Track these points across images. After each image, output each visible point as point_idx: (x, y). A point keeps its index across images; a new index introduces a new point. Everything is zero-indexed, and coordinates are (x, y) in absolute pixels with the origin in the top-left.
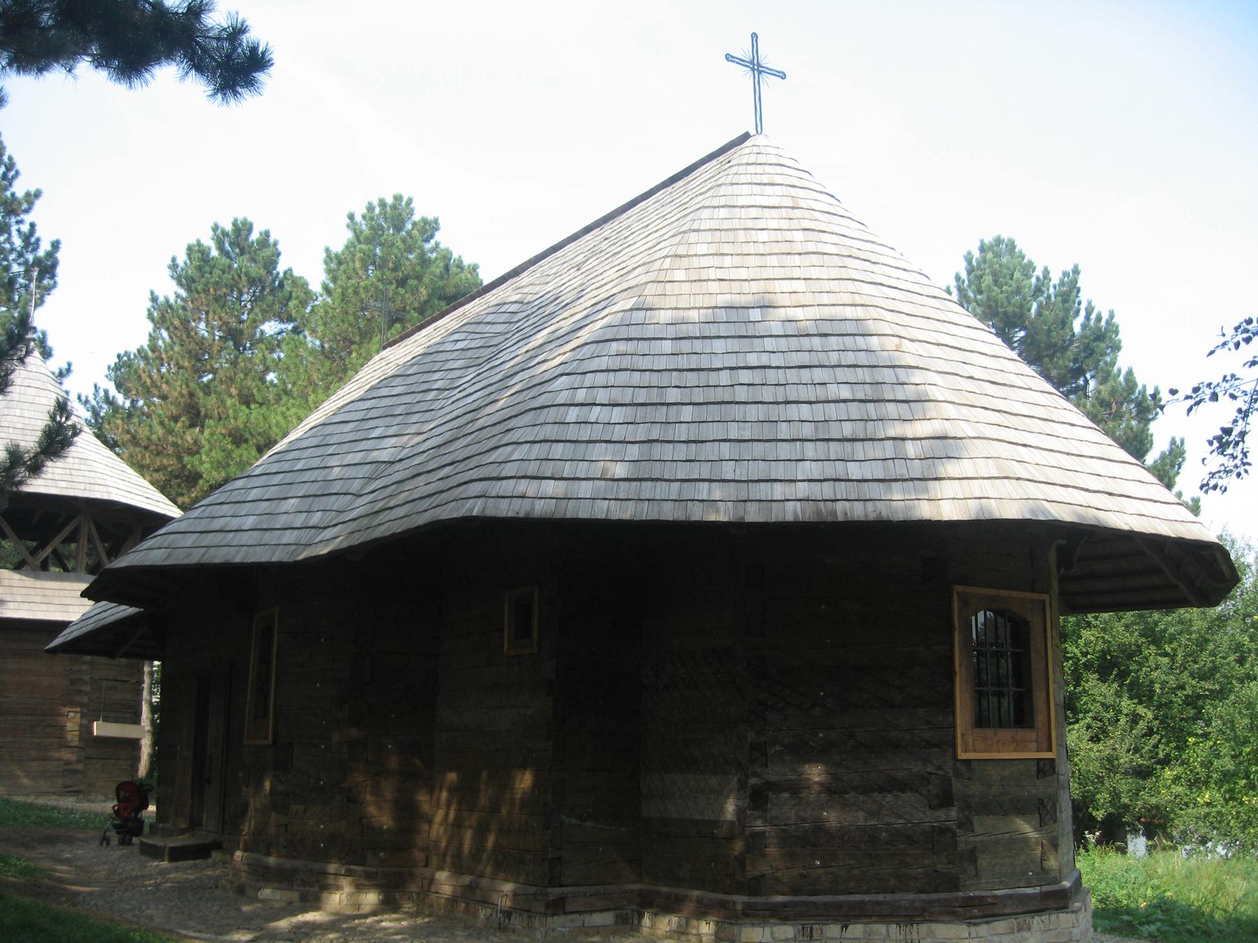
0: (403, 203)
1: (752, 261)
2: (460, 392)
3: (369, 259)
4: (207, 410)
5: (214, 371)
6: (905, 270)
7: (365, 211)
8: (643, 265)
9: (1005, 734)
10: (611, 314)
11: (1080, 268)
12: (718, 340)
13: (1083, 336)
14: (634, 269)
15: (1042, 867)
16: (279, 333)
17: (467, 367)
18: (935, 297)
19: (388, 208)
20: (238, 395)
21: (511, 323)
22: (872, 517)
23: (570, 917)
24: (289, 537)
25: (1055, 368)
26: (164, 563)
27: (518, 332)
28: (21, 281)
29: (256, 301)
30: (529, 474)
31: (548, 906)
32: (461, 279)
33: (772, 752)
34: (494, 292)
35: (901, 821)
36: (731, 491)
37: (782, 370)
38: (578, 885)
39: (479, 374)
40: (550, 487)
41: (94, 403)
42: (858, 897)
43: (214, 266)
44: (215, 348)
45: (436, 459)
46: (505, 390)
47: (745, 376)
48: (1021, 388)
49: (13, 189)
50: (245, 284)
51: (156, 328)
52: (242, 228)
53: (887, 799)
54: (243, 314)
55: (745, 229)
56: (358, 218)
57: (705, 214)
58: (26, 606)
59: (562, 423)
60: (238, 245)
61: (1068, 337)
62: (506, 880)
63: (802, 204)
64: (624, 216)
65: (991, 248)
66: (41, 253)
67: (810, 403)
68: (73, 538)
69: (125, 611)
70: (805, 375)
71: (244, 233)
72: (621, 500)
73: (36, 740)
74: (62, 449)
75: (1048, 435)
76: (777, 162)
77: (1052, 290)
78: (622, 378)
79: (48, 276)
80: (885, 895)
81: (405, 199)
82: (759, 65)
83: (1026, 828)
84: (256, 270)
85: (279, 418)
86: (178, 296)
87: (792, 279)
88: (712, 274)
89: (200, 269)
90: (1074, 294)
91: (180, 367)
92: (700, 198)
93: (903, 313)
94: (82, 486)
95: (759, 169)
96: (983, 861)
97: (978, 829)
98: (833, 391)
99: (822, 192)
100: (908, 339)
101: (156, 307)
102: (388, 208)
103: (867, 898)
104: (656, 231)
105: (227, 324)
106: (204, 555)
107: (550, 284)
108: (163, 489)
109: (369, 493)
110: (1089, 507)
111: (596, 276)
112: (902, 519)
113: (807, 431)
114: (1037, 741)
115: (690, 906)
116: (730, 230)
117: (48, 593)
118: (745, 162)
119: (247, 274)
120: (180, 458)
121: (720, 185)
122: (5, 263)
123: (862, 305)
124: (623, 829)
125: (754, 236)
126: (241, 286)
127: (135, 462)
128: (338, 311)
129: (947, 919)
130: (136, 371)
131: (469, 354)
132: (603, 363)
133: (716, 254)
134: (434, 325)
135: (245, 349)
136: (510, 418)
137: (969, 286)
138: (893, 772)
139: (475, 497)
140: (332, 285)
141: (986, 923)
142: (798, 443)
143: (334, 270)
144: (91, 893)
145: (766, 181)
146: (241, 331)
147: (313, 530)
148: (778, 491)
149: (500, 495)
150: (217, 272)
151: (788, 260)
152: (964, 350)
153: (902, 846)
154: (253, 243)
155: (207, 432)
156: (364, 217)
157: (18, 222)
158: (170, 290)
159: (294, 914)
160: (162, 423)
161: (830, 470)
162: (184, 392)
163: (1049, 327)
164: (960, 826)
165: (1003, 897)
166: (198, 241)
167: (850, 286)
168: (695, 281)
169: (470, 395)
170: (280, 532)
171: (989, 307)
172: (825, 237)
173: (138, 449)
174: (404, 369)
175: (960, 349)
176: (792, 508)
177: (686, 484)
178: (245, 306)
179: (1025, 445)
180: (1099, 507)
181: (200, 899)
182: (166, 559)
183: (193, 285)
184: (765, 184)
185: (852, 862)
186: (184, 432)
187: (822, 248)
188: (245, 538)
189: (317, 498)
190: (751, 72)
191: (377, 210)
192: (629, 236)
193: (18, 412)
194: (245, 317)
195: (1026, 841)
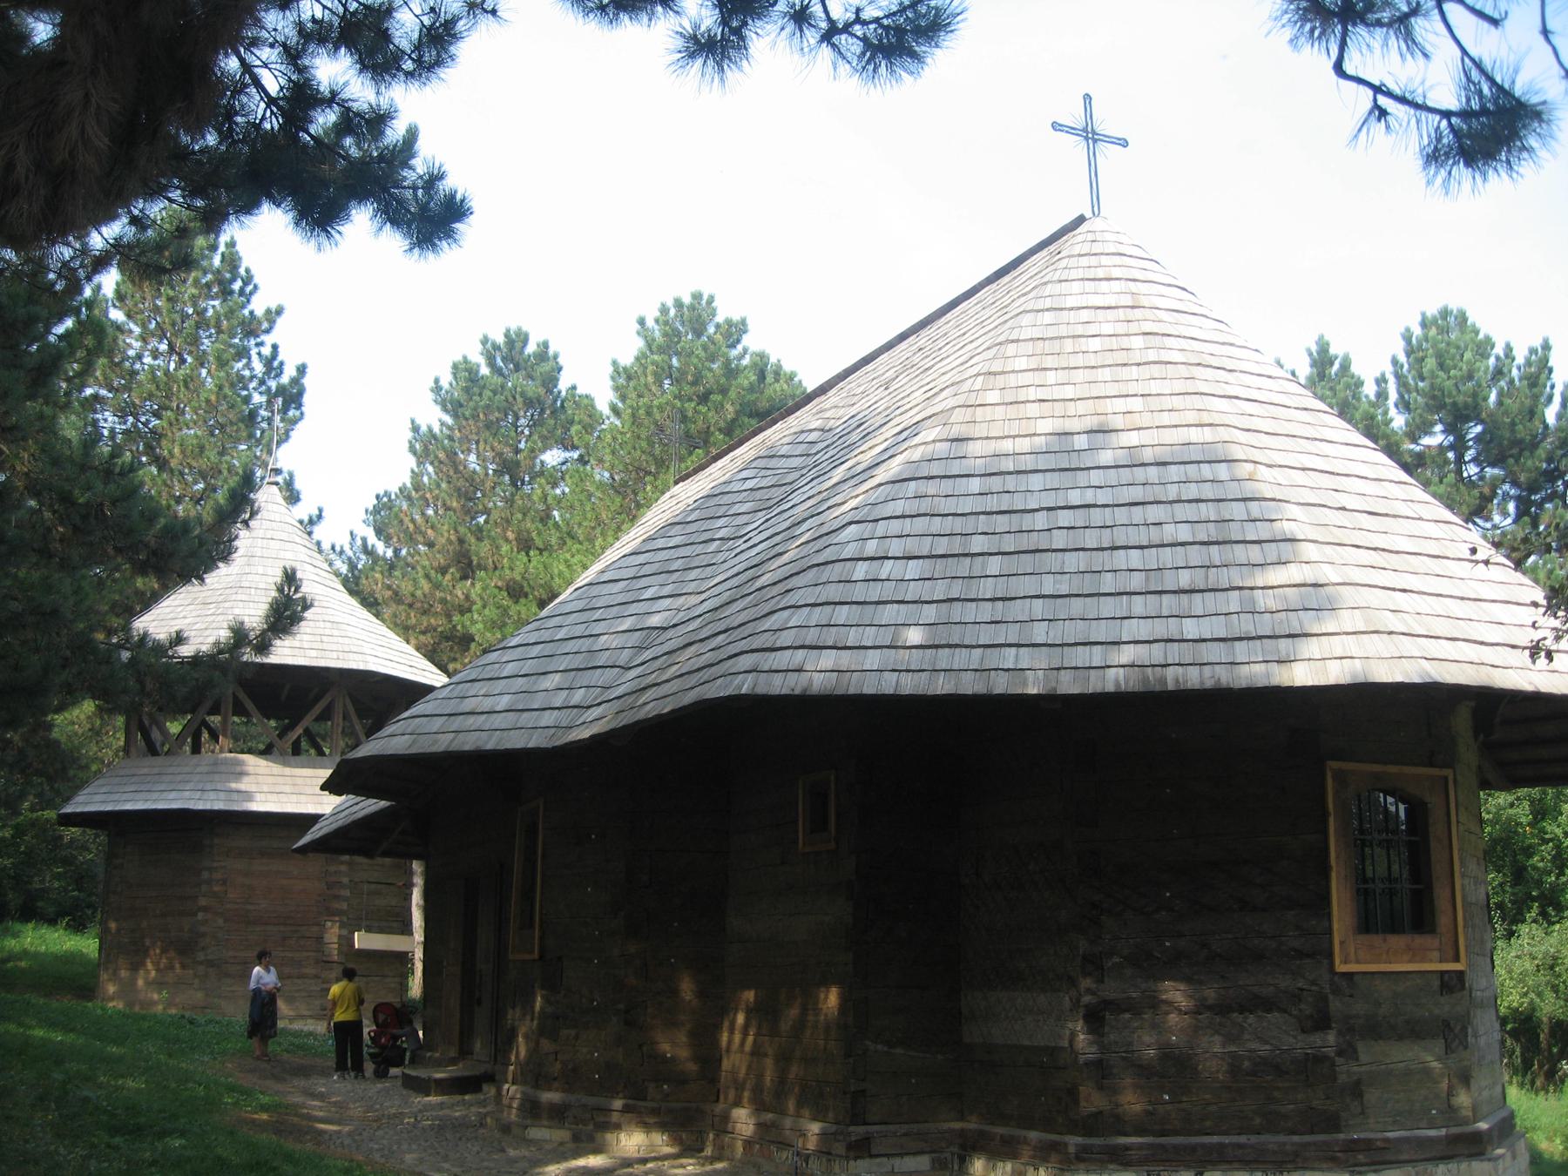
0: (704, 302)
1: (1080, 376)
2: (745, 542)
3: (663, 372)
4: (479, 558)
5: (487, 512)
6: (1270, 377)
7: (658, 314)
8: (952, 385)
9: (1397, 941)
10: (911, 447)
11: (1551, 342)
12: (1036, 475)
13: (1559, 429)
14: (942, 390)
15: (1449, 1106)
16: (563, 463)
17: (755, 512)
18: (1306, 409)
19: (685, 309)
20: (516, 539)
21: (808, 455)
22: (1209, 684)
23: (878, 1160)
24: (548, 718)
25: (1522, 471)
26: (407, 752)
27: (815, 467)
28: (263, 413)
29: (534, 425)
30: (807, 643)
31: (850, 1147)
32: (775, 391)
33: (1110, 964)
34: (798, 414)
35: (1268, 1047)
36: (1041, 659)
37: (1111, 509)
38: (886, 1123)
39: (767, 520)
40: (828, 659)
41: (350, 553)
42: (1215, 1139)
43: (484, 387)
44: (489, 484)
45: (712, 625)
46: (791, 541)
47: (1065, 518)
48: (1408, 518)
49: (250, 307)
50: (520, 406)
51: (419, 463)
52: (516, 340)
53: (1249, 1021)
54: (520, 442)
55: (1074, 337)
56: (650, 323)
57: (1027, 319)
58: (274, 797)
59: (848, 582)
60: (512, 360)
61: (1540, 431)
62: (815, 1119)
63: (1145, 301)
64: (943, 320)
65: (1434, 322)
66: (285, 379)
67: (1141, 547)
68: (325, 716)
69: (372, 805)
70: (1137, 514)
71: (518, 345)
72: (913, 671)
73: (289, 955)
74: (292, 625)
75: (1438, 576)
76: (1115, 251)
77: (1515, 372)
78: (920, 525)
79: (293, 406)
80: (1249, 1136)
81: (705, 297)
82: (1094, 133)
83: (1430, 1057)
84: (533, 388)
85: (562, 567)
86: (443, 424)
87: (1127, 396)
88: (1032, 394)
89: (467, 390)
90: (1543, 376)
91: (448, 509)
92: (1023, 299)
93: (1261, 432)
94: (335, 655)
95: (1093, 261)
96: (1372, 1096)
97: (1363, 1057)
98: (1169, 532)
99: (1170, 285)
100: (1265, 464)
101: (418, 437)
102: (685, 309)
103: (1227, 1140)
104: (972, 341)
105: (500, 454)
106: (452, 741)
107: (855, 407)
108: (432, 655)
109: (638, 665)
110: (1483, 664)
111: (903, 398)
112: (1244, 686)
113: (1137, 581)
114: (1440, 950)
115: (1026, 1152)
116: (1056, 338)
117: (299, 781)
118: (1076, 253)
119: (523, 394)
120: (449, 616)
121: (1046, 283)
122: (245, 393)
123: (1211, 425)
124: (940, 1057)
125: (1085, 344)
126: (516, 408)
127: (399, 622)
128: (628, 436)
129: (1325, 1166)
130: (396, 516)
131: (758, 495)
132: (898, 507)
133: (1037, 370)
134: (731, 454)
135: (523, 484)
136: (791, 575)
137: (1409, 371)
138: (1256, 987)
139: (745, 672)
140: (620, 405)
141: (1375, 1171)
142: (1125, 597)
143: (623, 386)
144: (339, 1132)
145: (1101, 275)
146: (518, 463)
147: (576, 710)
148: (1096, 656)
149: (773, 668)
150: (487, 393)
151: (1125, 373)
152: (1338, 474)
153: (1269, 1078)
154: (529, 356)
155: (478, 586)
156: (657, 321)
157: (258, 345)
158: (433, 417)
159: (566, 1159)
160: (427, 576)
161: (1160, 629)
162: (453, 538)
163: (1513, 420)
164: (1340, 1053)
165: (1399, 1140)
166: (465, 358)
167: (1198, 402)
168: (1011, 403)
169: (755, 545)
170: (538, 713)
171: (1434, 397)
172: (1169, 342)
173: (401, 608)
174: (684, 514)
175: (1333, 473)
176: (1113, 677)
177: (989, 651)
178: (522, 432)
179: (1404, 591)
180: (1496, 664)
181: (460, 1139)
182: (409, 747)
183: (459, 410)
184: (1100, 280)
185: (1207, 1096)
186: (454, 586)
187: (1165, 356)
188: (498, 721)
189: (580, 673)
190: (1084, 143)
191: (672, 312)
192: (944, 346)
193: (261, 570)
194: (522, 445)
195: (1427, 1072)
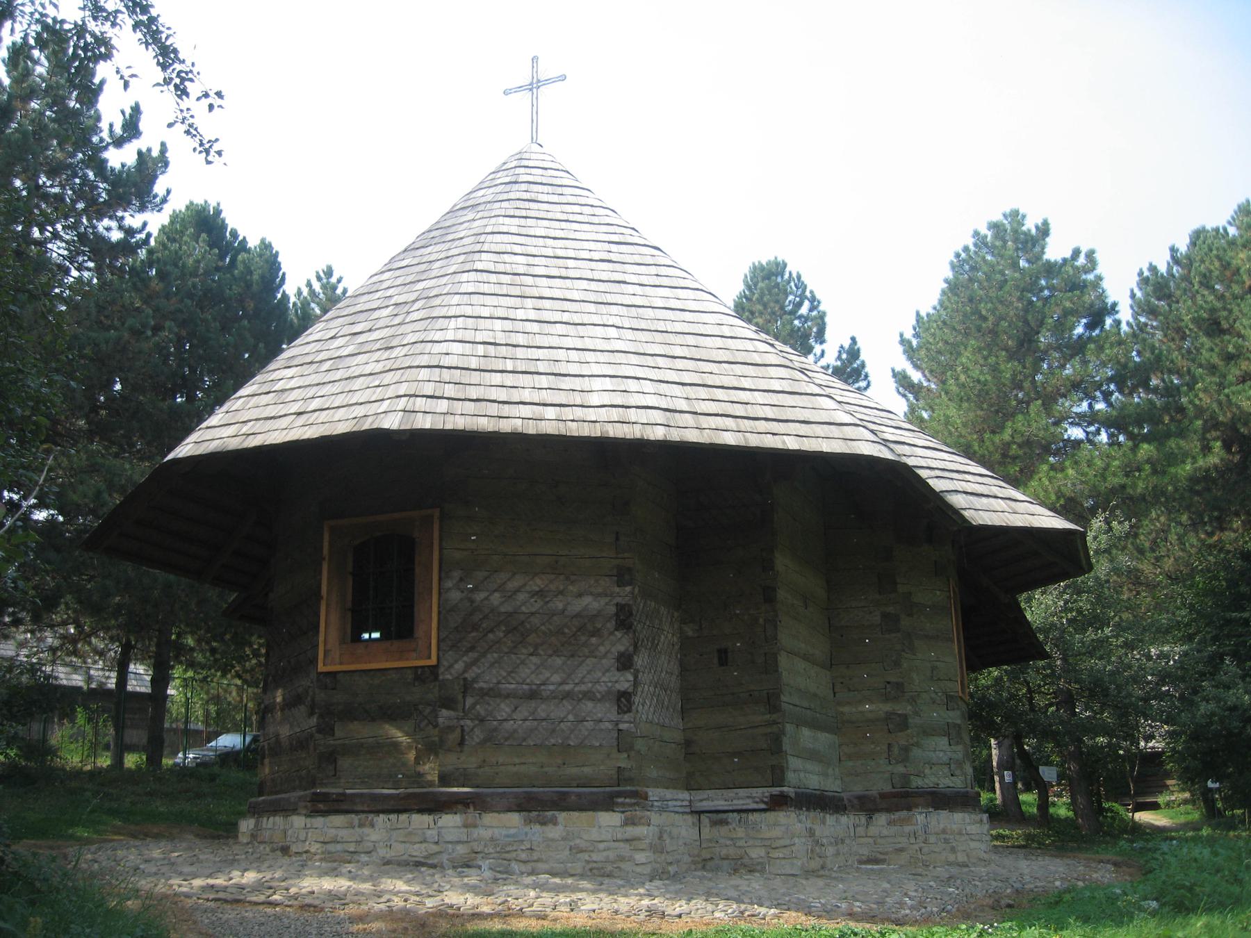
96: (345, 763)
195: (396, 745)
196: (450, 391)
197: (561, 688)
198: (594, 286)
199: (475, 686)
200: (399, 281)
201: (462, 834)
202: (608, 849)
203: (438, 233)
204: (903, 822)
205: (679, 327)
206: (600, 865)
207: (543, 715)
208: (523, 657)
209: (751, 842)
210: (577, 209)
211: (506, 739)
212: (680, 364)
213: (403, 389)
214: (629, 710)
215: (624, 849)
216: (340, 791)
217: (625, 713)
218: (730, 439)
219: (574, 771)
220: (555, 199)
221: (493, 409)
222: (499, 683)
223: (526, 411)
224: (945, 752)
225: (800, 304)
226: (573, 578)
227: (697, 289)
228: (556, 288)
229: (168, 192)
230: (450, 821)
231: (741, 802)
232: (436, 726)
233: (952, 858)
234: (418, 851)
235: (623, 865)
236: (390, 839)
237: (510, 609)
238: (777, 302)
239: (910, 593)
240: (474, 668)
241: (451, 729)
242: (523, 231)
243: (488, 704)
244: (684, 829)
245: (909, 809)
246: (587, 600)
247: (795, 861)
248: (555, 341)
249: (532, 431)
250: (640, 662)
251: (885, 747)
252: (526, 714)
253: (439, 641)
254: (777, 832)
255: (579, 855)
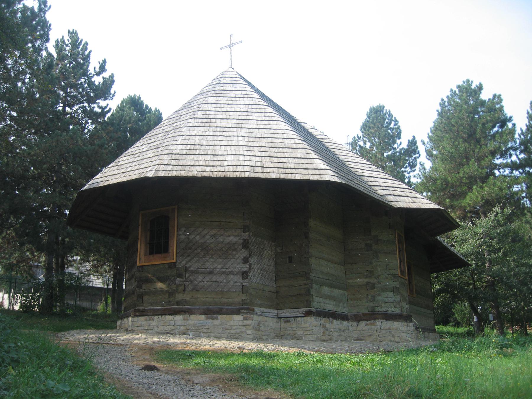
96: (146, 298)
196: (173, 162)
197: (221, 270)
198: (238, 121)
199: (190, 269)
200: (169, 123)
201: (183, 323)
202: (237, 329)
203: (188, 105)
204: (371, 324)
205: (267, 136)
206: (233, 334)
207: (215, 280)
208: (207, 259)
209: (298, 329)
210: (240, 92)
211: (201, 289)
212: (263, 149)
213: (157, 162)
214: (247, 278)
215: (243, 329)
216: (143, 308)
217: (245, 279)
218: (273, 176)
219: (226, 300)
220: (233, 89)
221: (187, 168)
222: (198, 268)
223: (199, 169)
224: (391, 298)
225: (390, 123)
226: (226, 230)
227: (279, 121)
228: (224, 123)
229: (115, 92)
230: (178, 318)
231: (295, 314)
232: (175, 284)
233: (393, 339)
234: (168, 328)
235: (242, 335)
236: (159, 325)
237: (203, 242)
238: (380, 122)
239: (377, 236)
240: (189, 263)
241: (180, 285)
242: (217, 102)
243: (194, 276)
244: (272, 323)
245: (374, 320)
246: (231, 238)
247: (314, 336)
248: (217, 143)
249: (200, 176)
250: (252, 261)
251: (366, 296)
252: (208, 279)
253: (176, 254)
254: (307, 325)
255: (226, 331)
